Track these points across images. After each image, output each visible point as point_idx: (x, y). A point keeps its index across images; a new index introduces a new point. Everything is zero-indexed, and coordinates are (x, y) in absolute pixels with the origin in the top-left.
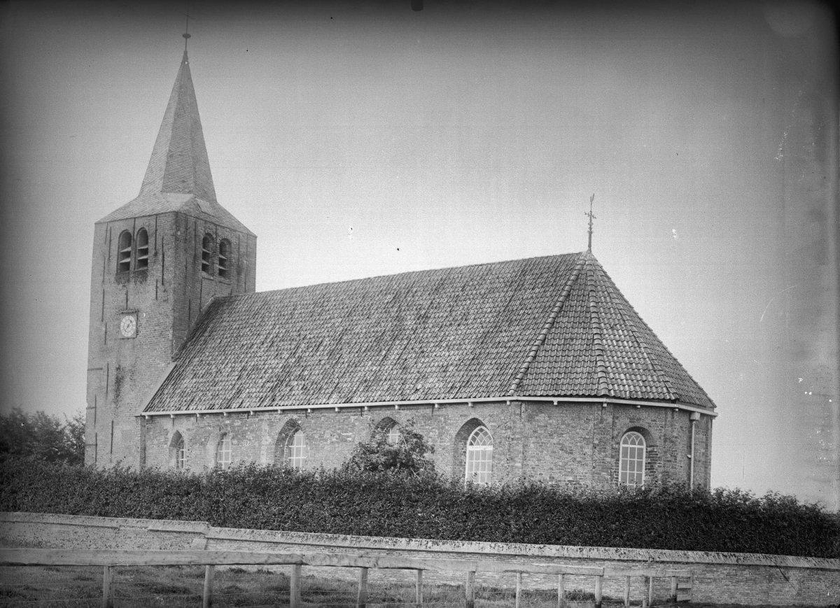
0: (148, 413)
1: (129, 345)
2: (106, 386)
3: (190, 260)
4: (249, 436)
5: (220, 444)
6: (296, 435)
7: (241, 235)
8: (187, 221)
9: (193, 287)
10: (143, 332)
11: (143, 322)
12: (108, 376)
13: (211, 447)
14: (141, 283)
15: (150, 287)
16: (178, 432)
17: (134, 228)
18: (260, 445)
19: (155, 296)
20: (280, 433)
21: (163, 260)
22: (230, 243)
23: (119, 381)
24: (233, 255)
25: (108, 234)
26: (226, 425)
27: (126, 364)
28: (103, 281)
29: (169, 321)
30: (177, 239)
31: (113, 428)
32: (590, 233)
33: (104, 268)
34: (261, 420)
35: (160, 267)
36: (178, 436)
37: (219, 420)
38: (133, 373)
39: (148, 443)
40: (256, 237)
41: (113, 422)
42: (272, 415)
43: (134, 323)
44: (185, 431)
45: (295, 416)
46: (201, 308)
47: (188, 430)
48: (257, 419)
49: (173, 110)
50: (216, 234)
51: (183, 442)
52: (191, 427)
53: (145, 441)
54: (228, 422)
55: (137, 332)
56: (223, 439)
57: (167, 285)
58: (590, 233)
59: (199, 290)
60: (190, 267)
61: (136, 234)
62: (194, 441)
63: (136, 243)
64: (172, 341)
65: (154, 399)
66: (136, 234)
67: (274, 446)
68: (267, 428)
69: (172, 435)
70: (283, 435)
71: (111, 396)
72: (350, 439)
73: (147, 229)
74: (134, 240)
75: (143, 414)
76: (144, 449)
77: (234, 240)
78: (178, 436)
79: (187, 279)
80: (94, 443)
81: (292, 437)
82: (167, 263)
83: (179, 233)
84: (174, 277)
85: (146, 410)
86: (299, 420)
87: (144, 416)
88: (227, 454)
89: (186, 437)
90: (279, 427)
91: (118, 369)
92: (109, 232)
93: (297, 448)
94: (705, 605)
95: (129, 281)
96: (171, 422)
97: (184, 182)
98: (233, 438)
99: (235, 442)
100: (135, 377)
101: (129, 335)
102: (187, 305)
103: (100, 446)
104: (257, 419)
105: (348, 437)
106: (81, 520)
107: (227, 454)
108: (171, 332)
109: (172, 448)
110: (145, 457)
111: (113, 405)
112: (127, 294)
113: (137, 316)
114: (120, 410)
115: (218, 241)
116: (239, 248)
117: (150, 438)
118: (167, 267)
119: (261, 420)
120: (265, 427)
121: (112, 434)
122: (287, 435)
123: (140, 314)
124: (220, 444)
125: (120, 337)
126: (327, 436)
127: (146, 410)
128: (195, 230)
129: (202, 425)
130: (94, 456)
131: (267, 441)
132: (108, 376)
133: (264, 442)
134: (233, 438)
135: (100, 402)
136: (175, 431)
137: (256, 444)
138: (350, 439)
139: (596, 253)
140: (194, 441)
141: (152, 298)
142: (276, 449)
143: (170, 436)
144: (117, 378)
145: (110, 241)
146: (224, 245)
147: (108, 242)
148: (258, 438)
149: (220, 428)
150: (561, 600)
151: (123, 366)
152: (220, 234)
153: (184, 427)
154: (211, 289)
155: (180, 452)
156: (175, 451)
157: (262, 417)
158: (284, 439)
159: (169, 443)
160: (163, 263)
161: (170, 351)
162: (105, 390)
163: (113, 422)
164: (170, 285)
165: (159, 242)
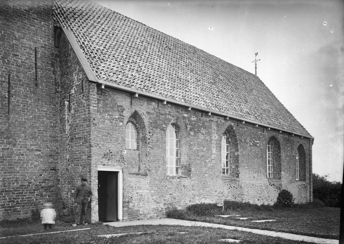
18: (211, 140)
32: (256, 68)
34: (212, 121)
37: (178, 112)
42: (219, 119)
44: (145, 113)
47: (148, 113)
48: (208, 119)
58: (256, 68)
72: (258, 145)
94: (311, 243)
104: (208, 119)
105: (257, 143)
106: (116, 224)
120: (214, 126)
126: (248, 141)
133: (213, 138)
138: (258, 145)
139: (258, 75)
148: (209, 134)
150: (105, 237)
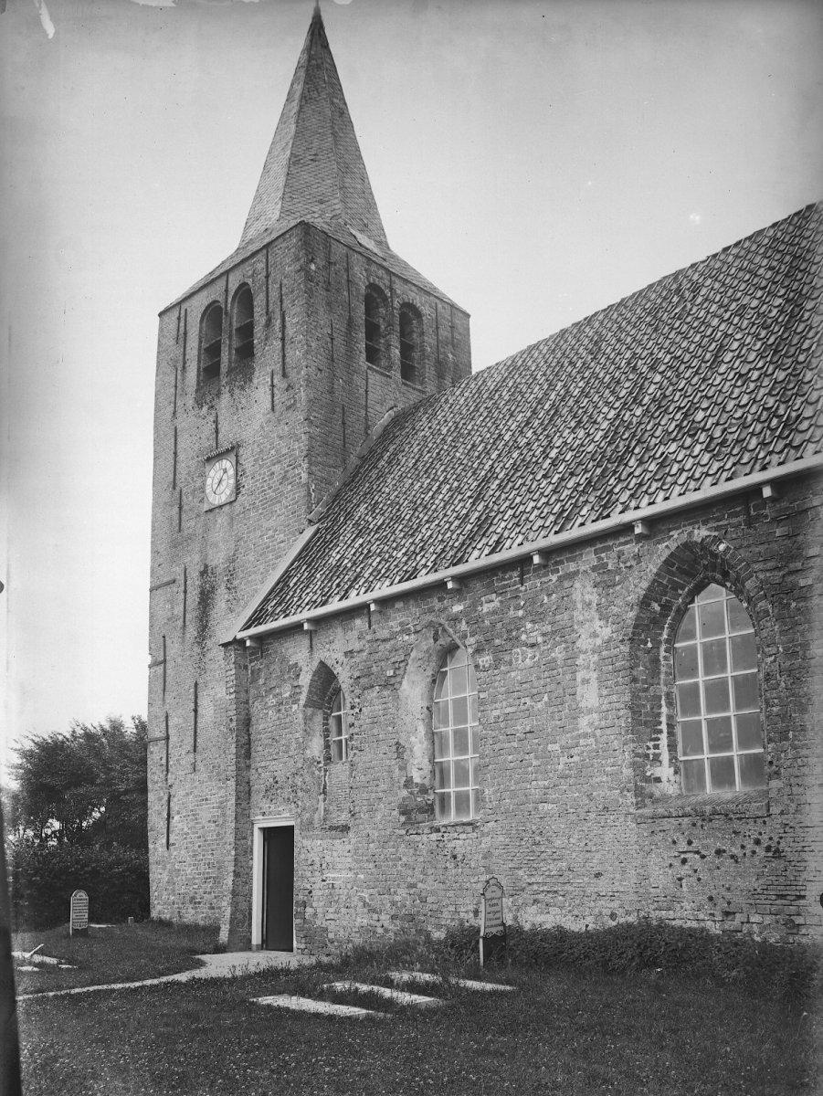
0: (253, 631)
1: (222, 519)
2: (181, 614)
3: (341, 326)
4: (531, 631)
5: (437, 679)
6: (700, 602)
7: (440, 306)
8: (328, 248)
9: (349, 382)
10: (247, 483)
11: (247, 464)
12: (185, 592)
13: (413, 690)
14: (242, 388)
15: (260, 393)
16: (322, 664)
17: (226, 291)
18: (571, 659)
19: (269, 406)
20: (644, 603)
21: (283, 327)
22: (419, 315)
23: (206, 598)
24: (426, 338)
25: (182, 324)
26: (455, 619)
27: (218, 559)
28: (174, 413)
29: (300, 447)
30: (309, 278)
31: (196, 697)
33: (176, 387)
35: (278, 344)
36: (325, 677)
37: (431, 610)
38: (231, 574)
39: (256, 707)
40: (468, 316)
41: (196, 684)
43: (231, 472)
44: (341, 657)
45: (701, 533)
46: (368, 427)
47: (349, 654)
49: (297, 96)
50: (391, 289)
51: (338, 691)
52: (357, 646)
53: (247, 702)
54: (457, 608)
55: (238, 488)
56: (444, 664)
57: (292, 374)
59: (362, 391)
60: (339, 341)
61: (230, 299)
62: (365, 679)
63: (231, 318)
64: (307, 485)
65: (266, 600)
66: (230, 299)
67: (625, 648)
68: (593, 596)
69: (309, 677)
70: (656, 607)
71: (192, 631)
73: (250, 281)
74: (226, 313)
75: (239, 636)
76: (246, 723)
77: (426, 310)
78: (325, 677)
79: (334, 363)
80: (163, 735)
81: (682, 612)
82: (290, 332)
83: (313, 267)
84: (307, 353)
85: (247, 627)
86: (717, 540)
87: (242, 642)
88: (460, 704)
89: (344, 677)
90: (637, 585)
91: (203, 573)
92: (182, 319)
93: (458, 795)
95: (219, 394)
96: (306, 642)
97: (321, 202)
98: (478, 651)
99: (486, 659)
100: (236, 583)
101: (223, 499)
102: (338, 416)
103: (173, 739)
104: (554, 578)
107: (460, 704)
108: (305, 466)
109: (309, 711)
110: (249, 743)
111: (197, 649)
112: (216, 422)
113: (237, 456)
114: (209, 656)
115: (396, 304)
116: (437, 328)
117: (258, 696)
118: (293, 343)
119: (572, 576)
120: (584, 592)
121: (196, 711)
122: (666, 608)
123: (241, 451)
124: (437, 679)
125: (206, 507)
127: (247, 627)
128: (347, 270)
129: (385, 634)
130: (164, 761)
131: (594, 635)
132: (185, 592)
133: (585, 643)
134: (478, 651)
135: (174, 649)
136: (316, 664)
137: (559, 654)
140: (365, 679)
141: (262, 414)
142: (633, 656)
143: (305, 679)
144: (202, 593)
145: (185, 334)
146: (410, 313)
147: (181, 340)
148: (562, 634)
149: (436, 633)
151: (212, 564)
152: (398, 292)
153: (336, 649)
154: (382, 395)
155: (332, 722)
156: (319, 718)
157: (572, 567)
158: (657, 622)
159: (303, 698)
160: (283, 334)
161: (304, 508)
162: (180, 623)
163: (196, 684)
164: (298, 373)
165: (274, 295)
